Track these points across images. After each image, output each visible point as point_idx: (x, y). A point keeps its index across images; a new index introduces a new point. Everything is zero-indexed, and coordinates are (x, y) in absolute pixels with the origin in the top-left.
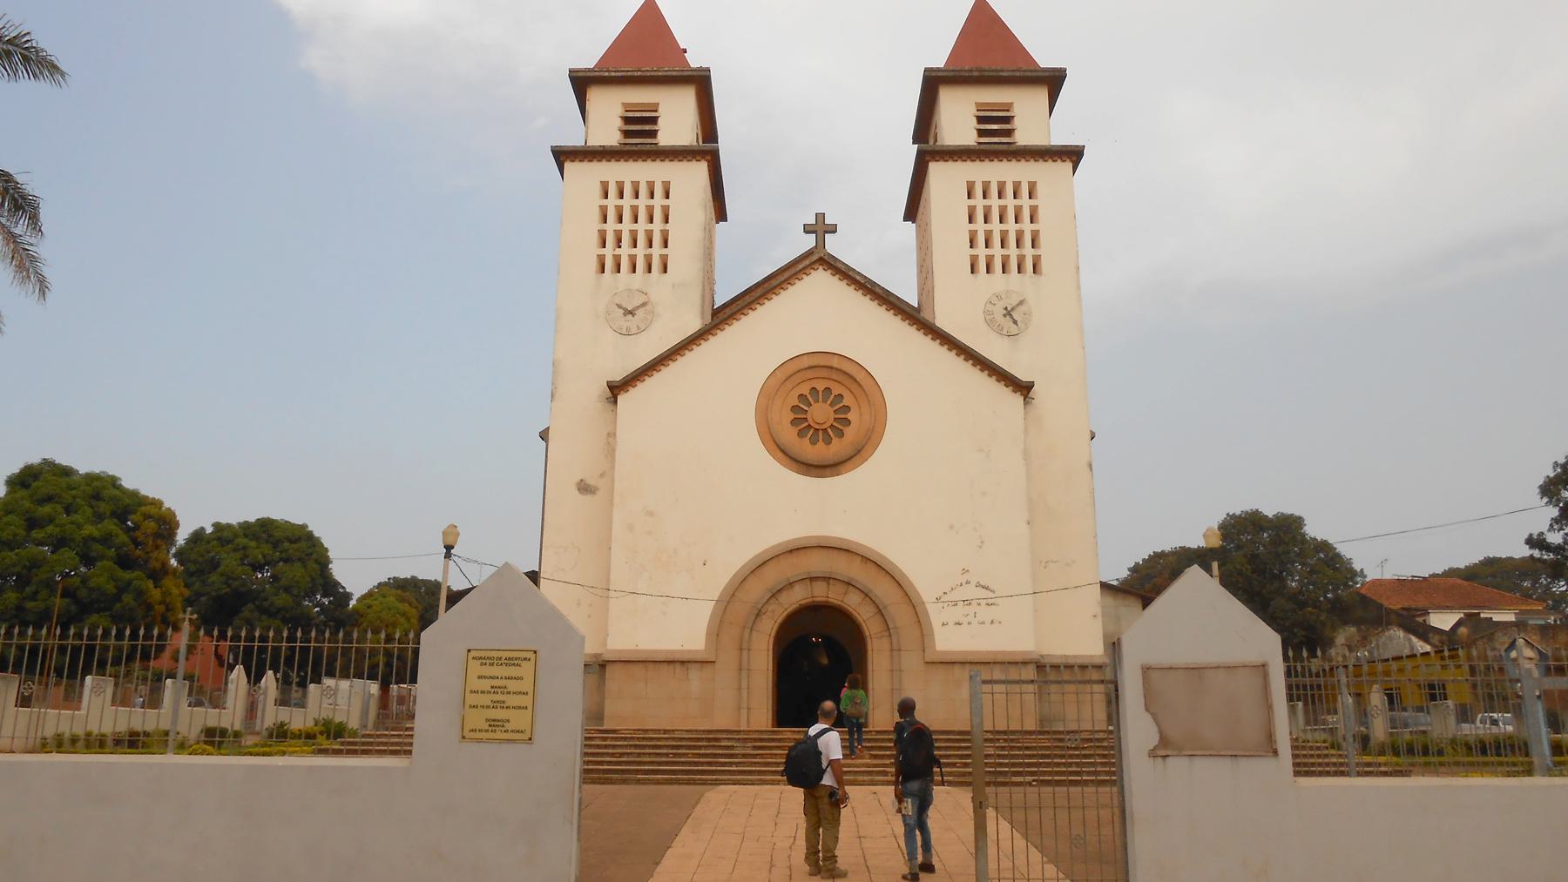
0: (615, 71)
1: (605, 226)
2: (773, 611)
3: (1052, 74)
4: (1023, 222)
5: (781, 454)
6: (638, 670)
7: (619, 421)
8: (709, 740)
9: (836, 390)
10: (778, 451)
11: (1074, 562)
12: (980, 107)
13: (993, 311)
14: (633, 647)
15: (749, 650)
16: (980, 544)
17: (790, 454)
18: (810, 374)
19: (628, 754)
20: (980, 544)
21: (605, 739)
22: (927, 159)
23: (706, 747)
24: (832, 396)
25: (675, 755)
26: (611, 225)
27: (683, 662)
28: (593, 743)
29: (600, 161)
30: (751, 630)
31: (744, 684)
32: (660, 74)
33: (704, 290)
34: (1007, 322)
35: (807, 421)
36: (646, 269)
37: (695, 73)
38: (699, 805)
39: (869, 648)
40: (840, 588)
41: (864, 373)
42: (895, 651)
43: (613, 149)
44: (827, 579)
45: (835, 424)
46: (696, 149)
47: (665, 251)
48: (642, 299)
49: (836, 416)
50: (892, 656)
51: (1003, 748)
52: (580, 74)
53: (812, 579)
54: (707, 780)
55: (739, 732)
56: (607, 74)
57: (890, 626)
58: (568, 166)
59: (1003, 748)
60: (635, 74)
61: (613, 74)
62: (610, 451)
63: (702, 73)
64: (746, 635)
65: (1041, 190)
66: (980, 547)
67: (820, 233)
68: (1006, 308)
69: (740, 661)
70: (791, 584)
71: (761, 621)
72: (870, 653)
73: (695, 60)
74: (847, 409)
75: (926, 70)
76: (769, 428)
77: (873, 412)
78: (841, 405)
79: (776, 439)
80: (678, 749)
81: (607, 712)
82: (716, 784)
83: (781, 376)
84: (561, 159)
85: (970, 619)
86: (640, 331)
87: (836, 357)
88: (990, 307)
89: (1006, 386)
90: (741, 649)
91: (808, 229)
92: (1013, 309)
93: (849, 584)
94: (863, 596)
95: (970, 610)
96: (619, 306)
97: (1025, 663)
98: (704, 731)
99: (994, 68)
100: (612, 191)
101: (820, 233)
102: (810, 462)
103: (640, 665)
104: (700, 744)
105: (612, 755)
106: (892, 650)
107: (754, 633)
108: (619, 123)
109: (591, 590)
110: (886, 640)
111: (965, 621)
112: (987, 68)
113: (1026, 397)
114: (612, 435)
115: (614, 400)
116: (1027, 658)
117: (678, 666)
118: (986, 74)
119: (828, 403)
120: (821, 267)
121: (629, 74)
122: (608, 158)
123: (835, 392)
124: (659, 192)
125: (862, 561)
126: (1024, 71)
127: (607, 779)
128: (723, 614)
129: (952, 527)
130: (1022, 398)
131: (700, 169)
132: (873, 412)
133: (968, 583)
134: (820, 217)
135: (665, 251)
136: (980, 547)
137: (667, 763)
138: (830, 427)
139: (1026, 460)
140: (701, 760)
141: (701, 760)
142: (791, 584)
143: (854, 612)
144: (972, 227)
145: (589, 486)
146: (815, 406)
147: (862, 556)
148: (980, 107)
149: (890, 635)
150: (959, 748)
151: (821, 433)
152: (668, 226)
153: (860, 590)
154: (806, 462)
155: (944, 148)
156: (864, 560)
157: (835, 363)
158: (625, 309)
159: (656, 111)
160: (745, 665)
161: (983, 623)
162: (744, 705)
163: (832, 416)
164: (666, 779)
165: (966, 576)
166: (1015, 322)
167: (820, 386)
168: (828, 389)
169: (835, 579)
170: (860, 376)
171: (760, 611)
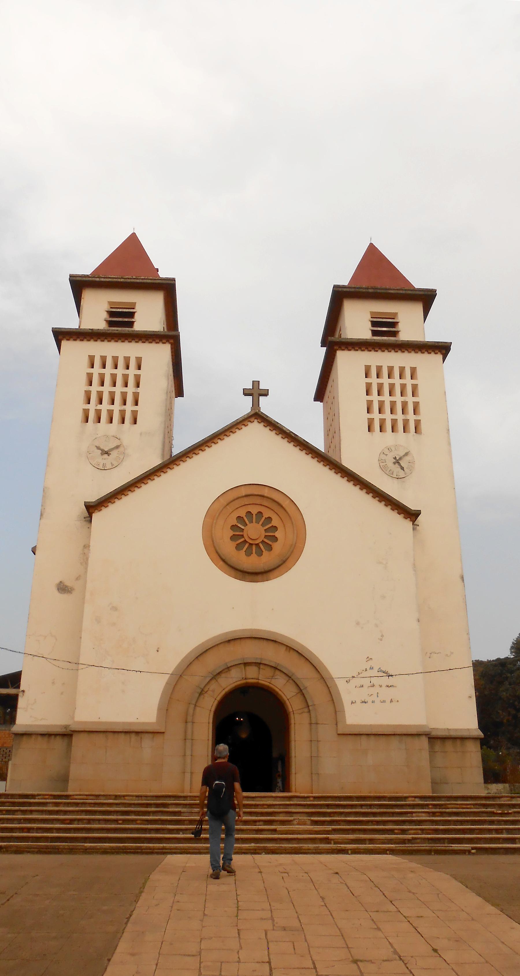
0: (104, 278)
1: (90, 388)
2: (213, 691)
3: (426, 293)
4: (407, 396)
5: (221, 563)
6: (100, 739)
7: (92, 533)
8: (157, 805)
9: (267, 513)
10: (220, 560)
11: (452, 653)
12: (374, 315)
13: (385, 460)
14: (97, 720)
15: (193, 723)
16: (380, 637)
17: (229, 563)
18: (246, 501)
19: (79, 820)
20: (380, 637)
21: (57, 804)
22: (335, 348)
23: (154, 813)
24: (263, 519)
25: (125, 821)
26: (95, 388)
27: (137, 733)
28: (45, 808)
29: (89, 340)
30: (195, 705)
31: (188, 753)
32: (138, 281)
33: (164, 438)
34: (396, 468)
35: (244, 537)
36: (120, 421)
37: (164, 282)
38: (143, 895)
39: (292, 721)
40: (268, 672)
41: (288, 501)
42: (313, 724)
43: (99, 331)
44: (258, 664)
45: (266, 540)
46: (162, 334)
47: (135, 408)
48: (116, 443)
49: (267, 534)
50: (311, 729)
51: (434, 814)
52: (78, 279)
53: (246, 664)
54: (154, 848)
55: (185, 797)
56: (98, 279)
57: (310, 704)
58: (64, 343)
59: (434, 814)
60: (119, 280)
61: (103, 280)
62: (85, 560)
63: (170, 282)
64: (191, 711)
65: (419, 373)
66: (381, 640)
67: (256, 395)
68: (395, 458)
69: (186, 732)
70: (228, 669)
71: (204, 698)
72: (292, 726)
73: (163, 274)
74: (275, 528)
75: (335, 287)
76: (213, 541)
77: (295, 532)
78: (270, 525)
79: (219, 551)
80: (128, 815)
81: (71, 776)
82: (164, 853)
83: (223, 501)
84: (60, 338)
85: (374, 698)
86: (113, 467)
87: (267, 488)
88: (383, 457)
89: (399, 514)
90: (186, 722)
91: (246, 392)
92: (400, 459)
93: (276, 668)
94: (287, 678)
95: (373, 691)
96: (98, 448)
97: (418, 735)
98: (153, 796)
99: (384, 287)
100: (97, 362)
101: (256, 395)
102: (245, 570)
103: (101, 735)
104: (149, 809)
105: (63, 821)
106: (311, 724)
107: (198, 709)
108: (105, 315)
109: (54, 662)
110: (306, 715)
111: (369, 700)
112: (379, 287)
113: (415, 526)
114: (87, 547)
115: (89, 519)
116: (421, 730)
117: (133, 735)
118: (378, 291)
119: (261, 523)
120: (256, 421)
121: (115, 280)
122: (96, 339)
123: (266, 515)
124: (133, 364)
125: (286, 649)
126: (406, 290)
127: (54, 848)
128: (172, 694)
129: (358, 624)
130: (412, 523)
131: (165, 349)
132: (295, 532)
133: (372, 668)
134: (256, 384)
135: (135, 408)
136: (381, 640)
137: (115, 830)
138: (261, 542)
139: (415, 571)
140: (149, 826)
141: (149, 826)
142: (228, 668)
143: (280, 693)
144: (369, 398)
145: (66, 586)
146: (250, 525)
147: (287, 646)
148: (374, 315)
149: (309, 712)
150: (393, 814)
151: (254, 547)
152: (139, 390)
153: (285, 673)
154: (242, 569)
155: (348, 341)
156: (288, 648)
157: (266, 492)
158: (102, 450)
159: (134, 309)
160: (189, 737)
161: (384, 702)
162: (188, 770)
163: (264, 534)
164: (112, 848)
165: (370, 663)
166: (402, 468)
167: (254, 510)
168: (260, 513)
169: (265, 664)
170: (286, 503)
171: (202, 690)
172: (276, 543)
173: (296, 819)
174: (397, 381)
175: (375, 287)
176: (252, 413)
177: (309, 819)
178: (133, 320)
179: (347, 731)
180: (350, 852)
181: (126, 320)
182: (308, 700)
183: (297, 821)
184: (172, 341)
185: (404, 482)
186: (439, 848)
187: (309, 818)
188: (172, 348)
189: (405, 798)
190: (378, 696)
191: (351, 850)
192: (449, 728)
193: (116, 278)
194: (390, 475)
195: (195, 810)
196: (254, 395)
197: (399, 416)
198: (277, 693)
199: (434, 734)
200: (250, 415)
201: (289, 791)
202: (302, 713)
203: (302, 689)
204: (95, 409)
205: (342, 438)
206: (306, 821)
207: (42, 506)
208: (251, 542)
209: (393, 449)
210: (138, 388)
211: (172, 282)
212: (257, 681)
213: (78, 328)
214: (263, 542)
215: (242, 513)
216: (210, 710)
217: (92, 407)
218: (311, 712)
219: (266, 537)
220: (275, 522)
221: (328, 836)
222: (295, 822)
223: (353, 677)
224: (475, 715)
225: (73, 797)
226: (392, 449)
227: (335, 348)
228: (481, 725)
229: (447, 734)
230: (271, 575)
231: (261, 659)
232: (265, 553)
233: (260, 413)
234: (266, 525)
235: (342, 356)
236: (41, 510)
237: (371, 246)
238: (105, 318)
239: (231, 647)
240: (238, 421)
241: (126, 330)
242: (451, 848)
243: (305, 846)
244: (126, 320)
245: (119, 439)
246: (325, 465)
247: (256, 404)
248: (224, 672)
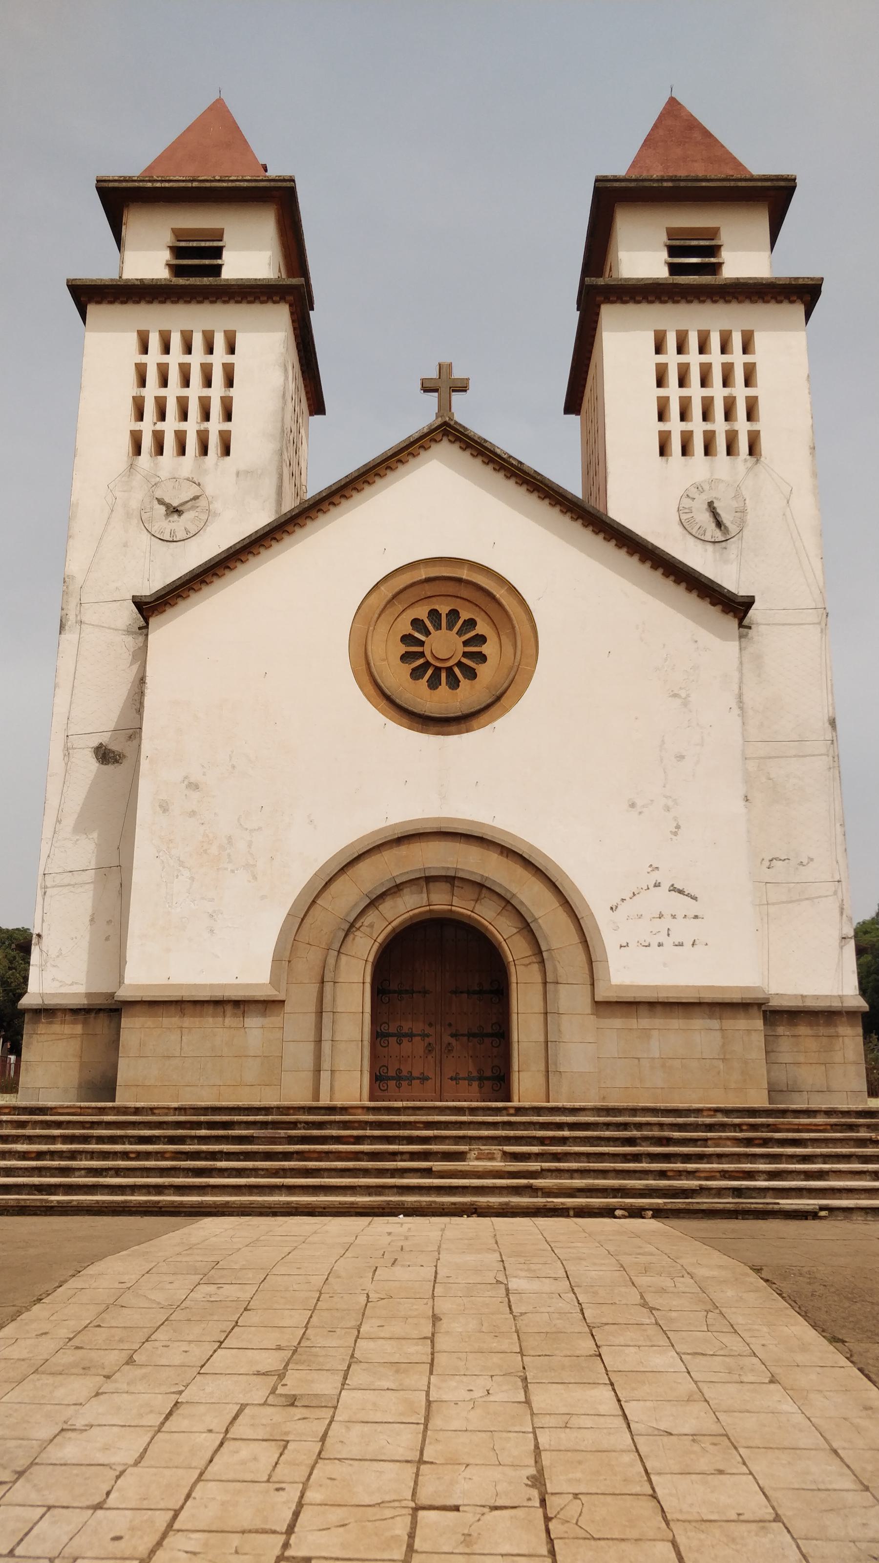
2: (371, 926)
13: (690, 508)
18: (429, 590)
22: (598, 299)
30: (339, 952)
39: (513, 979)
47: (226, 426)
48: (194, 491)
51: (749, 1142)
57: (543, 948)
58: (91, 309)
64: (331, 961)
66: (675, 834)
67: (444, 389)
71: (354, 939)
74: (481, 639)
83: (387, 592)
85: (662, 937)
91: (426, 385)
93: (481, 886)
96: (161, 502)
101: (444, 389)
107: (343, 958)
108: (166, 255)
116: (749, 996)
118: (682, 184)
123: (465, 615)
130: (735, 623)
136: (675, 834)
142: (397, 886)
152: (232, 392)
157: (465, 574)
158: (168, 506)
161: (681, 945)
170: (500, 593)
172: (483, 665)
173: (474, 1149)
174: (715, 358)
175: (676, 176)
176: (439, 421)
177: (500, 1150)
178: (219, 262)
179: (612, 996)
180: (571, 1213)
181: (207, 262)
182: (539, 941)
183: (476, 1152)
184: (290, 298)
185: (726, 548)
186: (753, 1206)
187: (500, 1147)
188: (292, 314)
189: (698, 1112)
190: (668, 935)
191: (574, 1209)
192: (805, 993)
193: (183, 181)
194: (699, 537)
195: (280, 1133)
196: (442, 390)
197: (719, 425)
198: (486, 928)
199: (774, 1003)
200: (433, 427)
201: (509, 1099)
202: (530, 964)
203: (529, 921)
204: (153, 431)
205: (608, 470)
206: (494, 1153)
207: (62, 609)
208: (438, 664)
209: (706, 487)
210: (231, 389)
211: (288, 184)
212: (449, 907)
213: (118, 278)
214: (459, 664)
215: (421, 612)
216: (366, 961)
217: (147, 427)
218: (546, 962)
219: (465, 655)
220: (482, 628)
221: (532, 1181)
222: (472, 1155)
223: (623, 900)
224: (853, 972)
225: (55, 1111)
226: (704, 487)
227: (598, 299)
228: (863, 990)
229: (800, 1004)
230: (474, 723)
231: (456, 869)
232: (464, 683)
233: (452, 423)
234: (453, 626)
235: (609, 314)
236: (61, 617)
237: (673, 102)
238: (167, 261)
239: (403, 850)
240: (412, 440)
241: (206, 281)
242: (776, 1206)
243: (482, 1200)
244: (207, 262)
245: (199, 485)
246: (575, 517)
247: (445, 406)
248: (389, 892)
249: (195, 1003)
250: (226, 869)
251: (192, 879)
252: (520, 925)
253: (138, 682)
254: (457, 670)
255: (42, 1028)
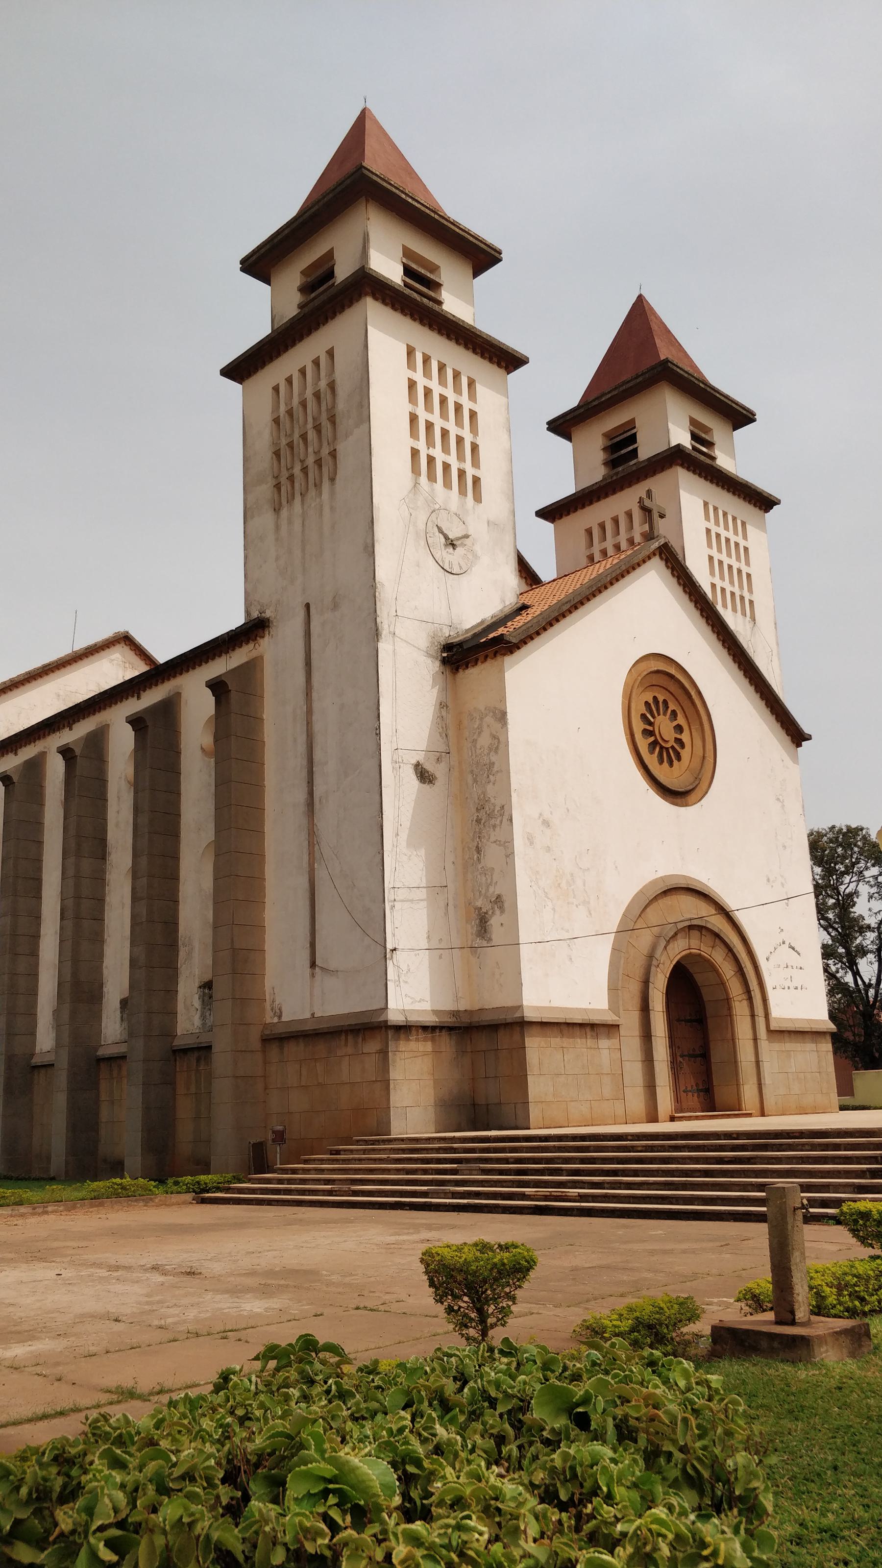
193: (427, 207)
249: (568, 1024)
250: (573, 903)
251: (554, 909)
252: (736, 969)
253: (438, 707)
254: (671, 751)
255: (403, 1045)
